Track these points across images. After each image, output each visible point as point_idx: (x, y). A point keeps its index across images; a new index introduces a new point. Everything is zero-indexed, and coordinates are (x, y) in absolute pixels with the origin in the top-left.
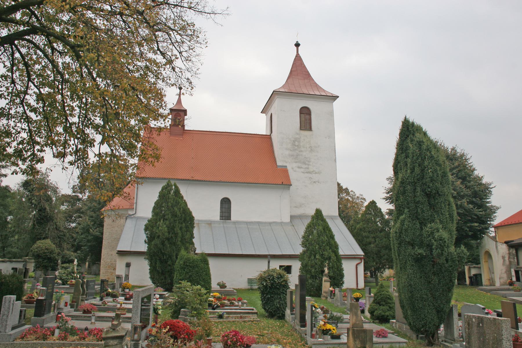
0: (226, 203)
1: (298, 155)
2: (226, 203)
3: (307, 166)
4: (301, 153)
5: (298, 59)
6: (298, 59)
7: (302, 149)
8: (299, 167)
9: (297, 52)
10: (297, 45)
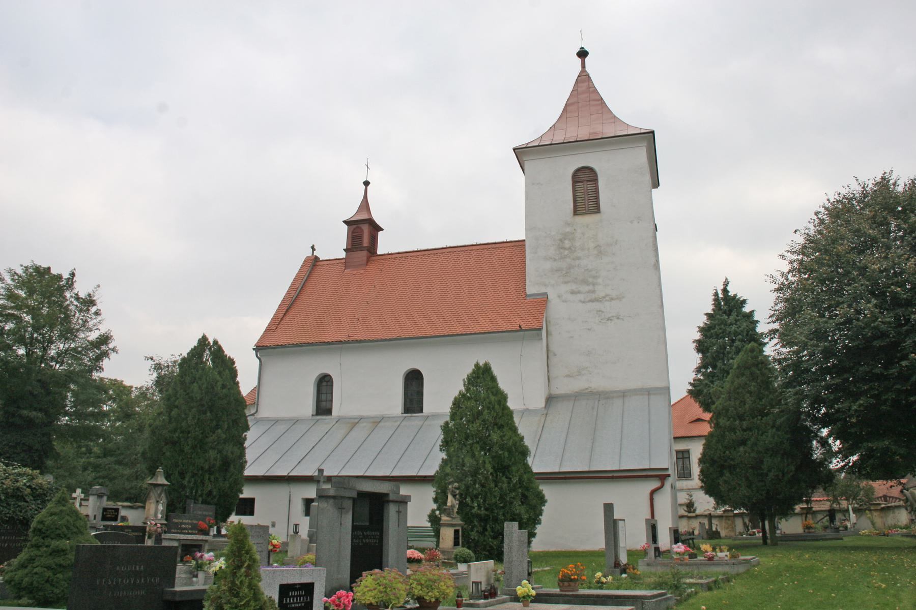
0: (324, 383)
1: (570, 267)
2: (324, 383)
3: (591, 287)
4: (577, 262)
5: (584, 78)
6: (584, 78)
7: (580, 253)
8: (573, 292)
9: (583, 66)
10: (583, 54)
